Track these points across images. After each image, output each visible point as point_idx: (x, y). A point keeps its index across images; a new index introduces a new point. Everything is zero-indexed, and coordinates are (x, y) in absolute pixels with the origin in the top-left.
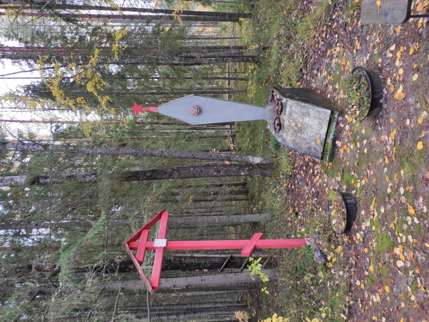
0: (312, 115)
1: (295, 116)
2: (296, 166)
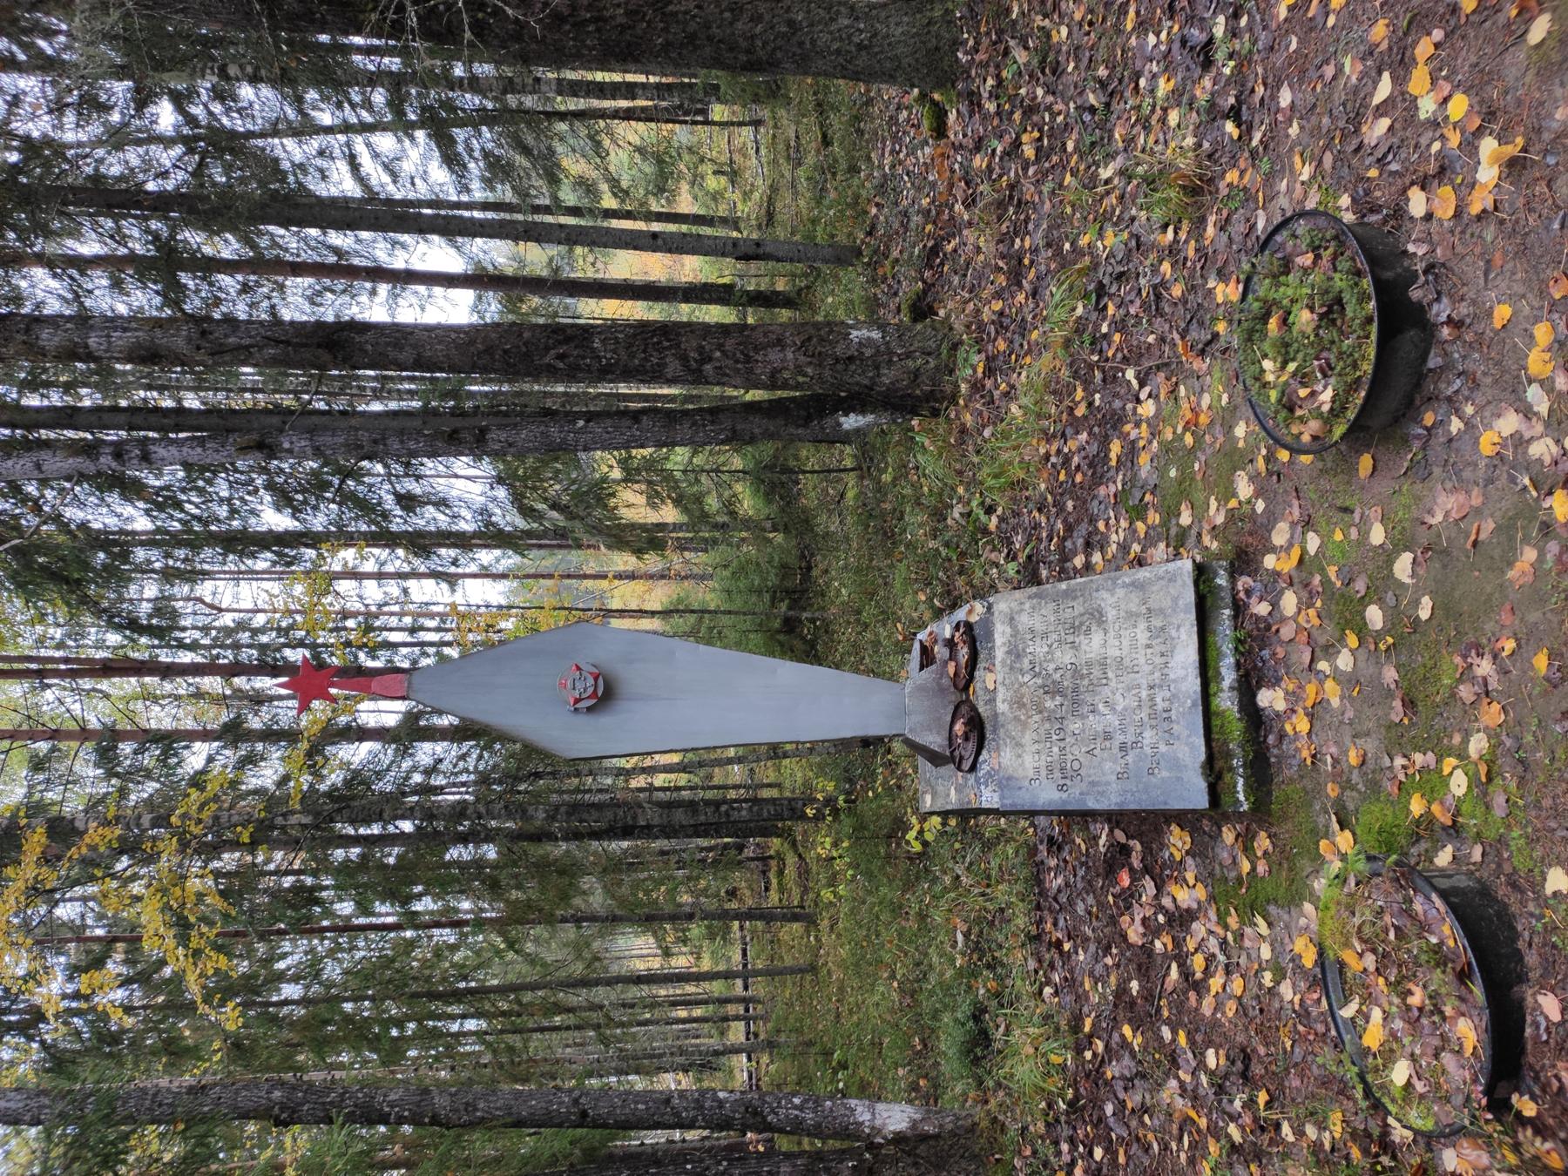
0: (1111, 614)
1: (1039, 649)
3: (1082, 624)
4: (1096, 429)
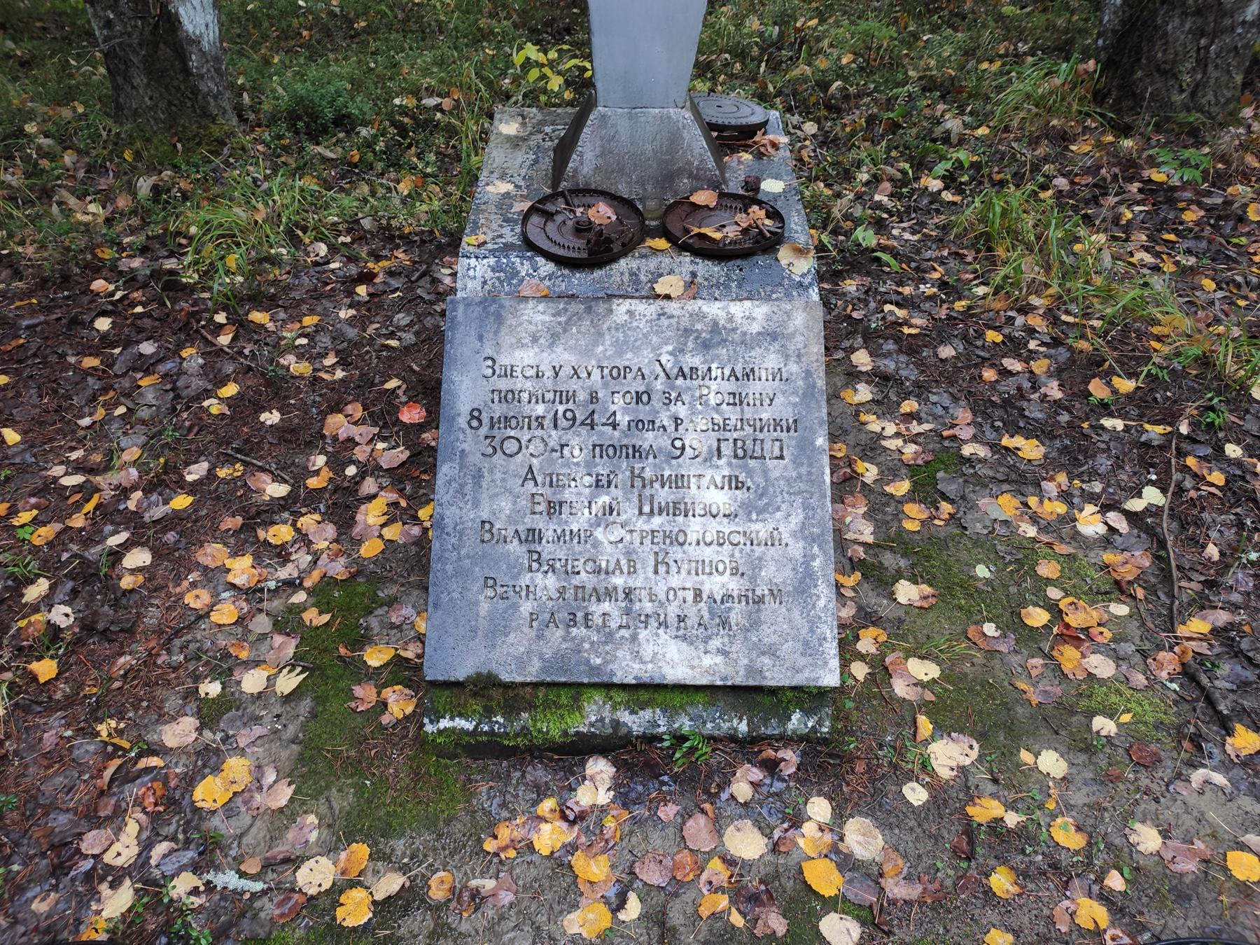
0: (761, 529)
2: (258, 317)
3: (750, 473)
4: (1064, 418)
